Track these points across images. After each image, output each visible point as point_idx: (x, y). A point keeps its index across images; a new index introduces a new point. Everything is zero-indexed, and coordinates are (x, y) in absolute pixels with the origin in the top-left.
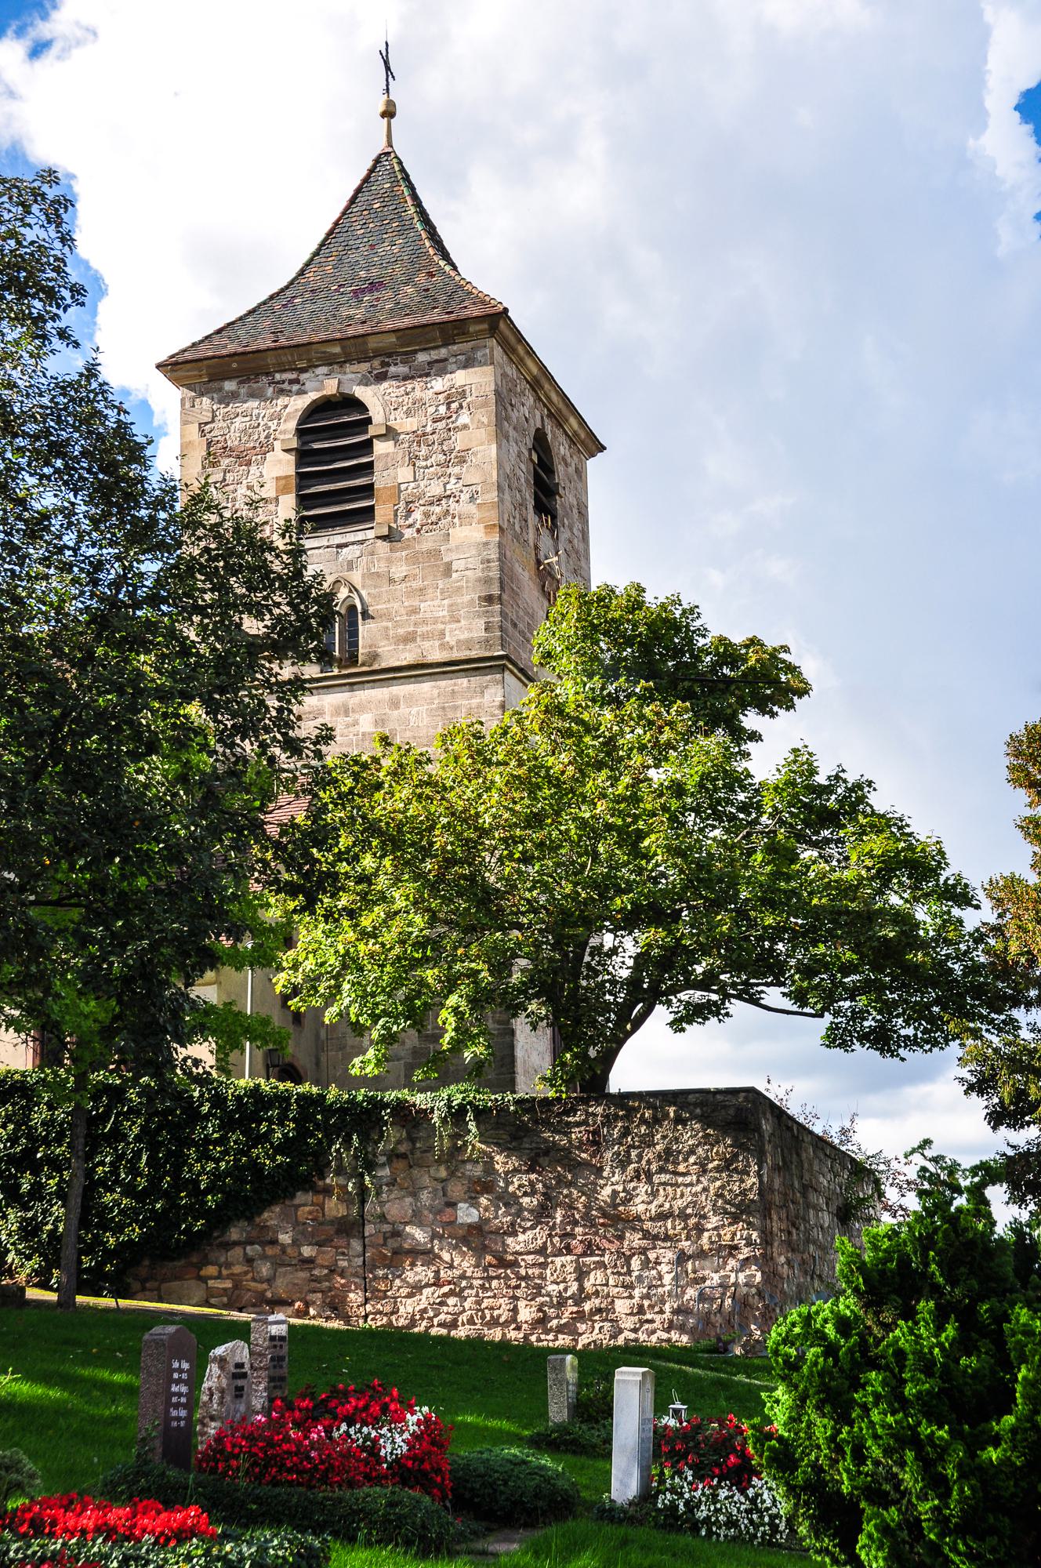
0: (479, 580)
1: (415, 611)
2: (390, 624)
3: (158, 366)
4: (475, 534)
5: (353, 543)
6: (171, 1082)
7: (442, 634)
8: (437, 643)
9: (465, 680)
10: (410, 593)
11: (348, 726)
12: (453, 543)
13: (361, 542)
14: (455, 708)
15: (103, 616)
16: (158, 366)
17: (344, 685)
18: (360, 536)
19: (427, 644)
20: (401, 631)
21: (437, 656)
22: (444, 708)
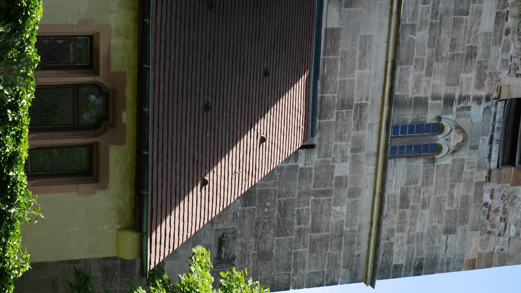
0: (436, 258)
1: (424, 206)
2: (419, 184)
3: (374, 288)
4: (471, 252)
5: (491, 150)
6: (3, 130)
7: (401, 230)
8: (395, 227)
9: (383, 226)
10: (440, 201)
11: (343, 152)
12: (469, 233)
13: (489, 157)
14: (339, 246)
15: (253, 277)
16: (374, 288)
17: (378, 148)
18: (495, 156)
19: (396, 218)
20: (411, 195)
21: (386, 225)
22: (341, 236)
